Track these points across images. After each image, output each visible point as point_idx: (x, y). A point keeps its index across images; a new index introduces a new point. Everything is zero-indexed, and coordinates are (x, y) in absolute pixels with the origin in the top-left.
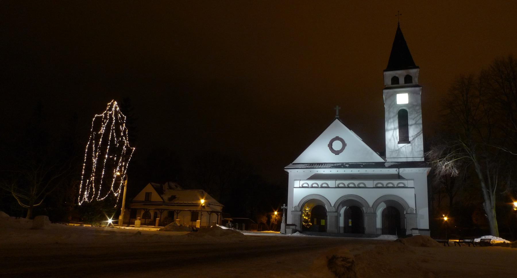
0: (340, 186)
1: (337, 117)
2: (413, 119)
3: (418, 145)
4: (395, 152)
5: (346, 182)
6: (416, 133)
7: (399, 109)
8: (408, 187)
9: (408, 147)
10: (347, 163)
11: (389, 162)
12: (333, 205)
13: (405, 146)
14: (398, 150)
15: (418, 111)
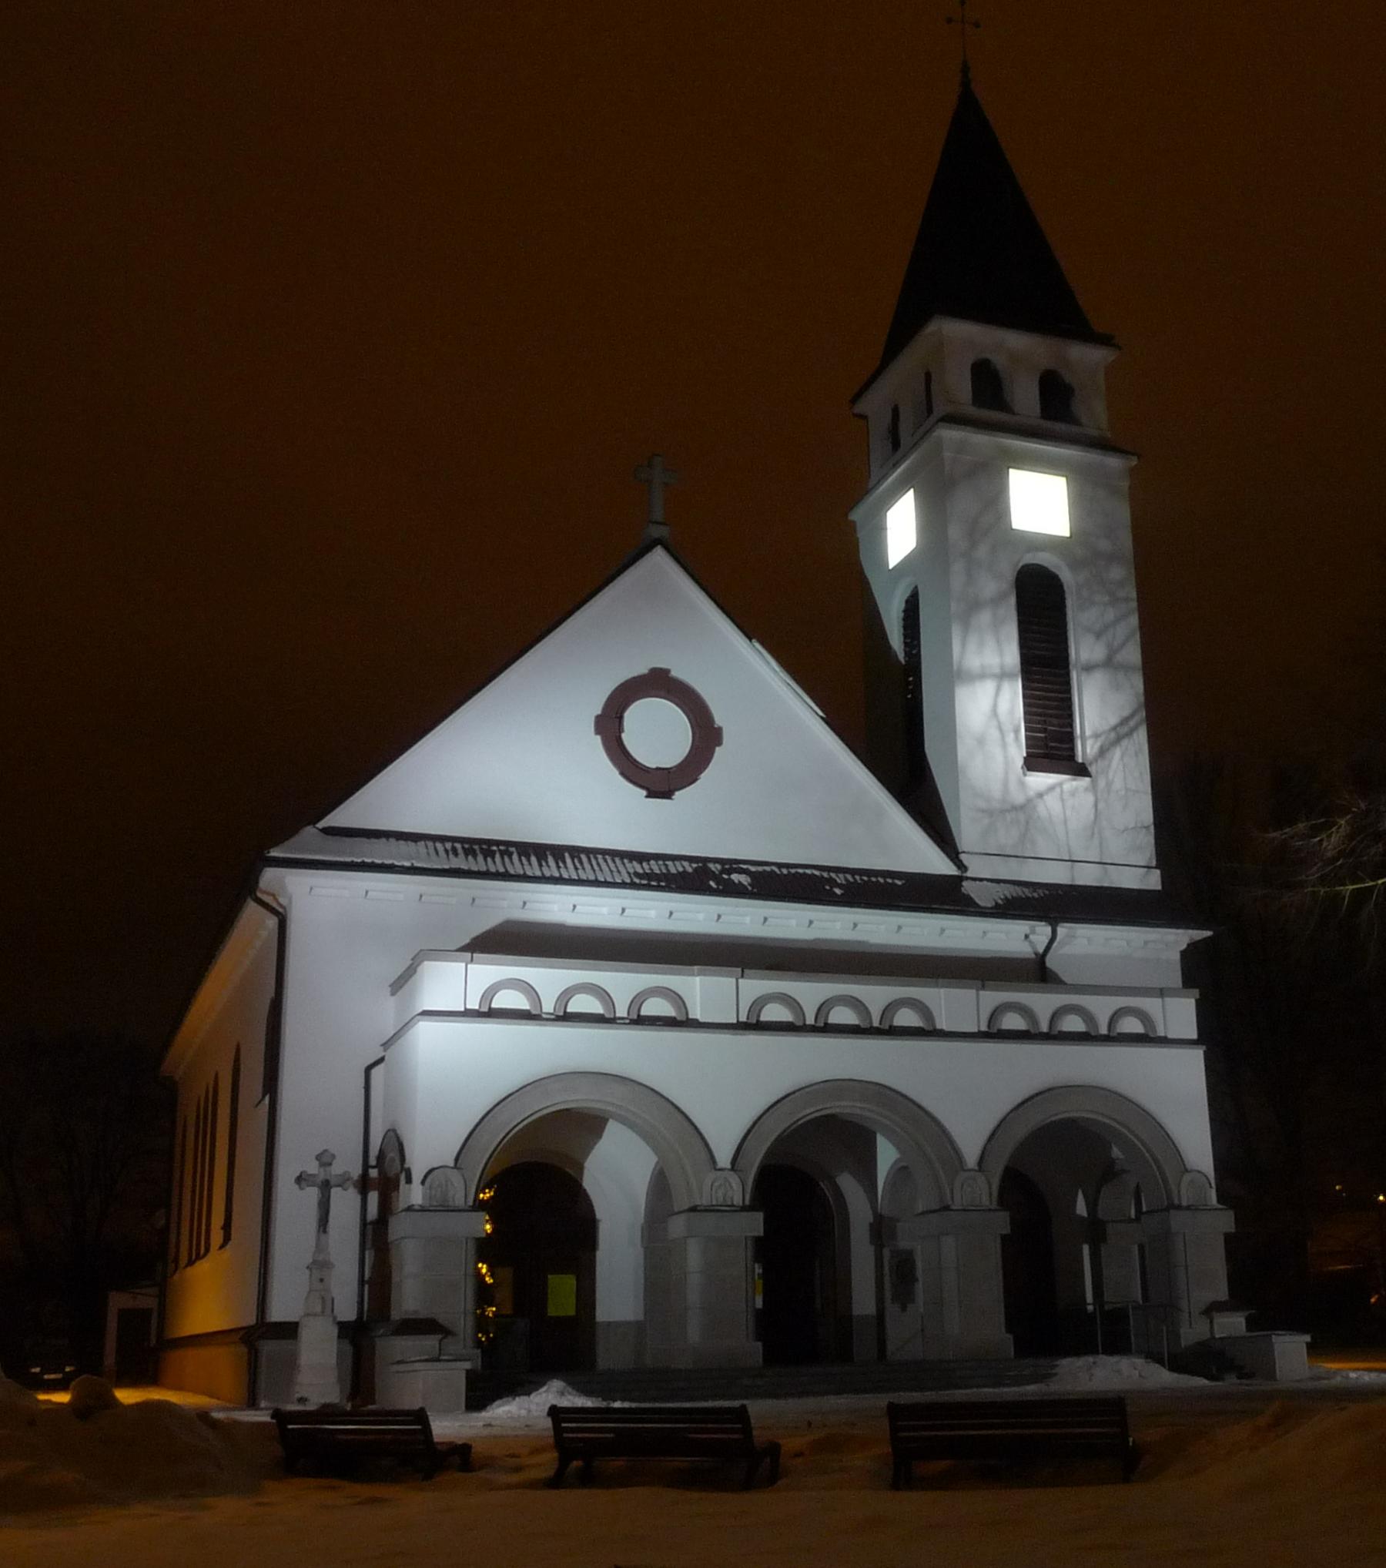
0: (503, 1001)
1: (656, 532)
2: (1098, 635)
3: (1127, 790)
4: (1009, 817)
5: (810, 993)
6: (1113, 720)
7: (1019, 561)
8: (1170, 1036)
9: (1073, 793)
10: (732, 865)
11: (981, 880)
12: (971, 1156)
13: (1058, 790)
14: (1021, 808)
15: (1121, 594)
